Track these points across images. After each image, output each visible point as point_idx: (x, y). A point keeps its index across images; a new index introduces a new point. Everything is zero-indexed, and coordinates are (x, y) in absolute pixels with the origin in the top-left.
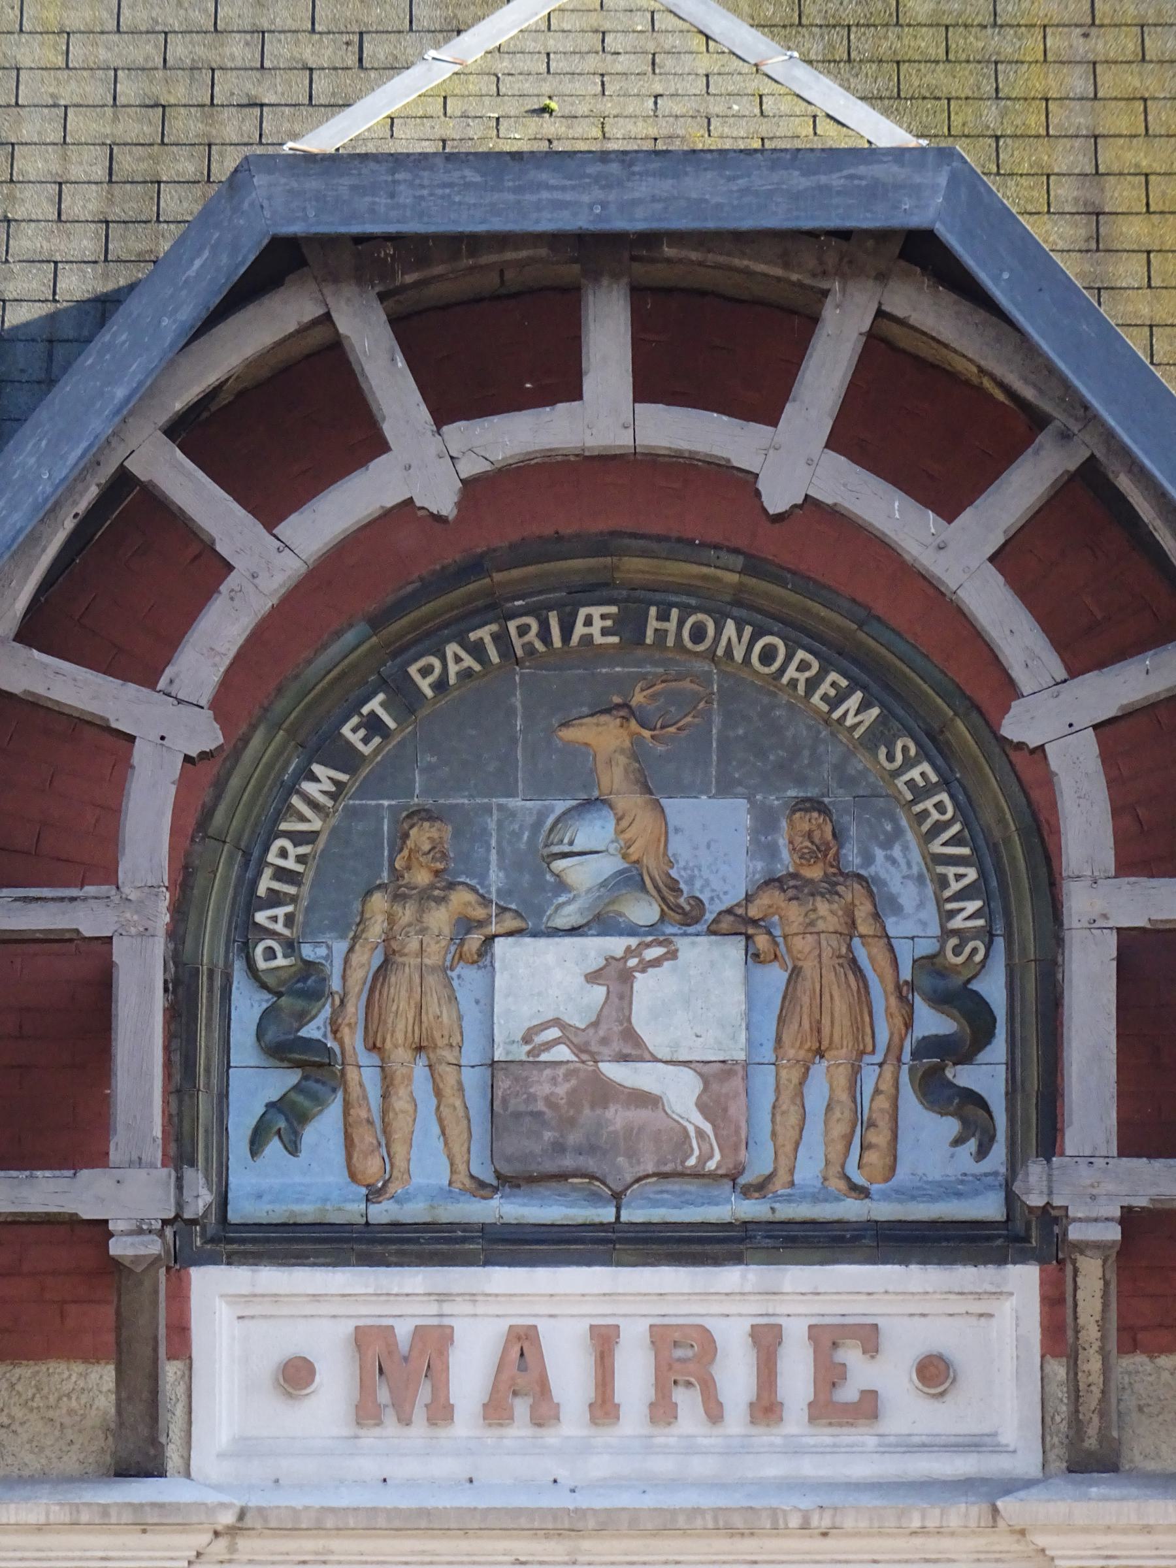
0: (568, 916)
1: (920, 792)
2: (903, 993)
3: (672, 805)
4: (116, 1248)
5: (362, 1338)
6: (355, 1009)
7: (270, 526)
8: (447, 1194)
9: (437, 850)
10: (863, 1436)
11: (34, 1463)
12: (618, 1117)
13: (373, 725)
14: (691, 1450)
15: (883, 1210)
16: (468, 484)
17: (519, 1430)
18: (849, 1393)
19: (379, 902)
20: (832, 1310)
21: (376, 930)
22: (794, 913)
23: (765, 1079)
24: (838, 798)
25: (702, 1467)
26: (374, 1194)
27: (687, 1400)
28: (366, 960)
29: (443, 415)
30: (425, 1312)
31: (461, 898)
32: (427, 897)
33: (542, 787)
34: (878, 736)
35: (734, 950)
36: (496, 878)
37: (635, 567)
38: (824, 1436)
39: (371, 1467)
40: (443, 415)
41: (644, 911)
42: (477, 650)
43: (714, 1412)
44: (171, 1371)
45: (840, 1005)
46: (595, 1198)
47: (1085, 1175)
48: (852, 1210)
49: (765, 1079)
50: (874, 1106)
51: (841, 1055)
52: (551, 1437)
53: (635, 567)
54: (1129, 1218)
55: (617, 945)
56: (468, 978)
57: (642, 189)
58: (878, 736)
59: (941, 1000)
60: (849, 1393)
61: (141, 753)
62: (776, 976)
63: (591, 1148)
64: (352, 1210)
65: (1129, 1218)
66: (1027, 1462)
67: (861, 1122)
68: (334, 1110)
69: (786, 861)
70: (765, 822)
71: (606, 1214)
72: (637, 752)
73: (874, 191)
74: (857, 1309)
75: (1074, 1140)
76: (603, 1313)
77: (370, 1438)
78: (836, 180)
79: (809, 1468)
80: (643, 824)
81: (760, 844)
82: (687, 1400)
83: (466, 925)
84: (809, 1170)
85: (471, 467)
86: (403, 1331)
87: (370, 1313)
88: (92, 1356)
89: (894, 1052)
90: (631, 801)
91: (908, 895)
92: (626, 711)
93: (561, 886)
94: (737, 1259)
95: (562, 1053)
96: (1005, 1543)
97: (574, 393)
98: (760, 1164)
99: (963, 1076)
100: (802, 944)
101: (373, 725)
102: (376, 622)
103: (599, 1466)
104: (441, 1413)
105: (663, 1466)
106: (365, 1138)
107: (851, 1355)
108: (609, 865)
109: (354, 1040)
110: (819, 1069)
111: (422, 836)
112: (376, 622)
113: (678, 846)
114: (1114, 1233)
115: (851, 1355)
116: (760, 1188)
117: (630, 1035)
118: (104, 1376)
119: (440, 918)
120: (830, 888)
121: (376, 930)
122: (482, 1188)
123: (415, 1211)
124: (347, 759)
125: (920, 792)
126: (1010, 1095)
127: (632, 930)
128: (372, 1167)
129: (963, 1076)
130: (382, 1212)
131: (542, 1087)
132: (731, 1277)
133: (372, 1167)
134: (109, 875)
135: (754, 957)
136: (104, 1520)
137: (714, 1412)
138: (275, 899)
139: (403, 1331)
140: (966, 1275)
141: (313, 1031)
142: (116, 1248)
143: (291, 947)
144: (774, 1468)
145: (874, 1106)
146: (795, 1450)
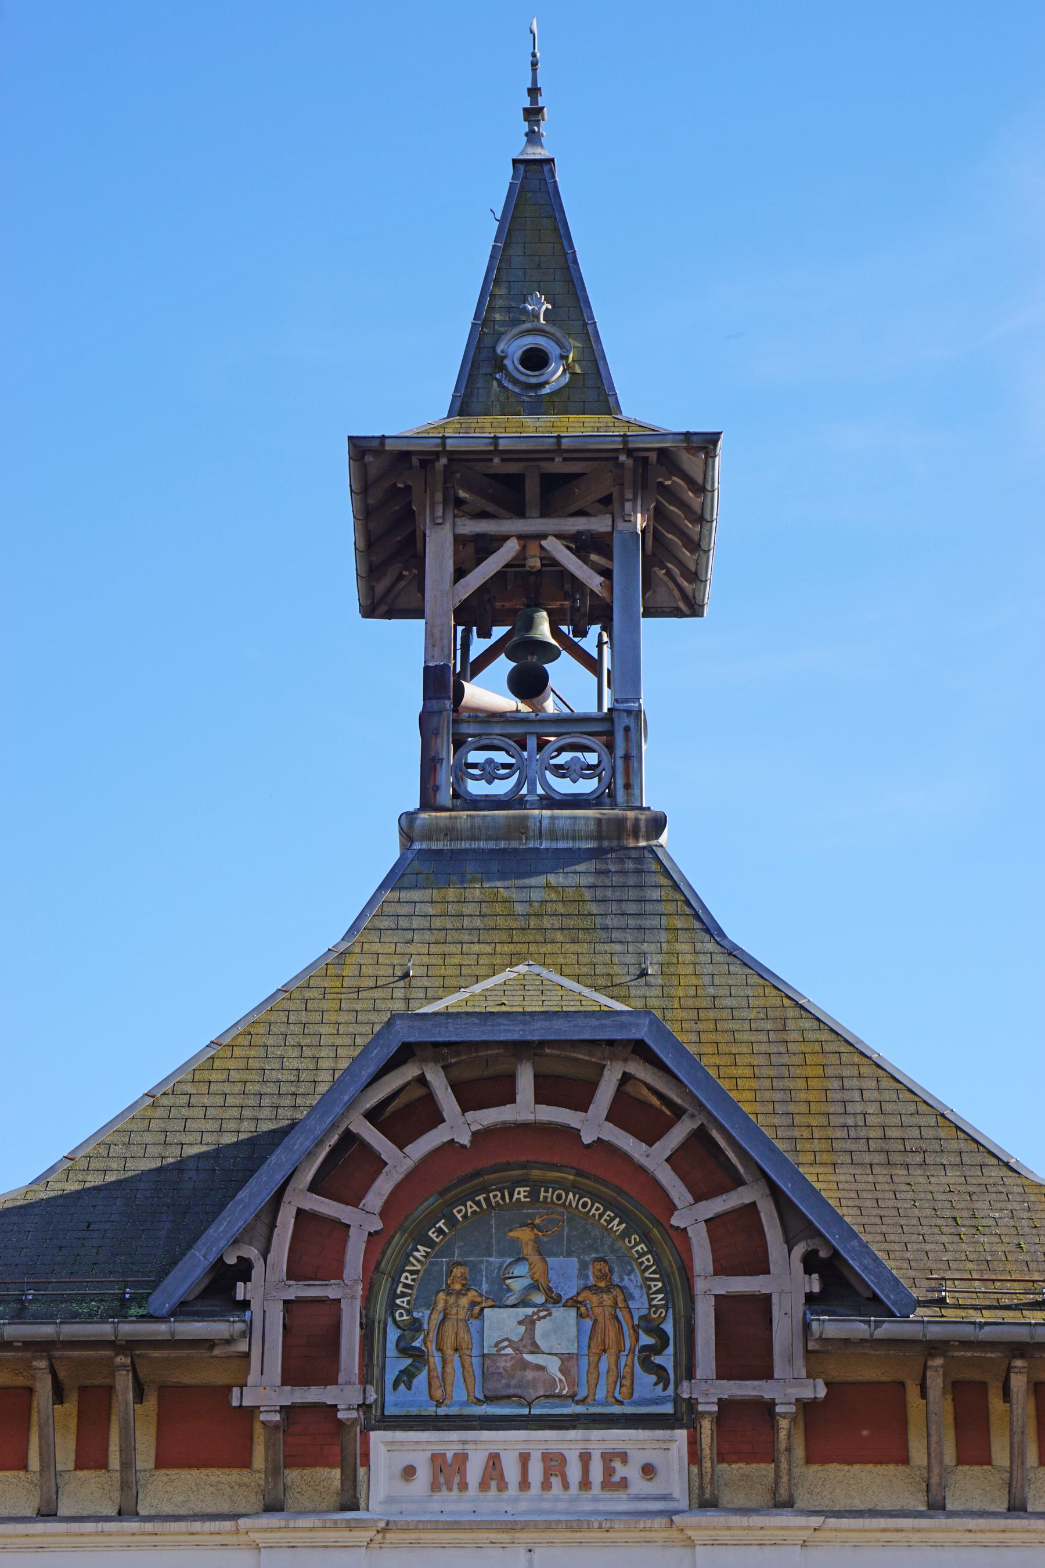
0: (512, 1300)
1: (641, 1255)
2: (635, 1329)
3: (550, 1260)
4: (341, 1415)
5: (434, 1457)
6: (433, 1335)
7: (401, 1148)
8: (466, 1404)
9: (463, 1277)
10: (621, 1495)
11: (309, 1506)
12: (530, 1375)
13: (440, 1231)
14: (556, 1500)
15: (628, 1410)
16: (475, 1134)
17: (493, 1492)
18: (616, 1478)
19: (442, 1295)
20: (610, 1446)
21: (440, 1306)
22: (595, 1299)
23: (584, 1362)
24: (610, 1257)
25: (561, 1506)
26: (439, 1404)
27: (556, 1481)
28: (437, 1317)
29: (464, 1109)
30: (458, 1448)
31: (472, 1294)
32: (459, 1294)
33: (501, 1254)
34: (626, 1234)
35: (573, 1313)
36: (485, 1287)
37: (536, 1173)
38: (607, 1495)
39: (436, 1507)
40: (464, 1109)
41: (539, 1298)
42: (478, 1204)
43: (566, 1486)
44: (362, 1471)
45: (612, 1334)
46: (522, 1406)
47: (704, 1386)
48: (617, 1409)
49: (584, 1362)
50: (625, 1371)
51: (613, 1351)
52: (505, 1495)
53: (536, 1173)
54: (721, 1402)
55: (529, 1311)
56: (474, 1324)
57: (538, 1025)
58: (626, 1234)
59: (649, 1332)
60: (616, 1478)
61: (352, 1231)
62: (588, 1323)
63: (520, 1386)
64: (431, 1410)
65: (721, 1402)
66: (684, 1504)
67: (620, 1377)
68: (424, 1373)
69: (592, 1281)
70: (584, 1266)
71: (526, 1411)
72: (537, 1241)
73: (623, 1026)
74: (619, 1446)
75: (699, 1373)
76: (524, 1448)
77: (437, 1496)
78: (607, 1022)
79: (601, 1507)
80: (539, 1267)
81: (582, 1274)
82: (556, 1481)
83: (473, 1304)
84: (601, 1394)
85: (475, 1127)
86: (450, 1455)
87: (437, 1448)
88: (332, 1466)
89: (632, 1350)
90: (535, 1258)
91: (636, 1292)
92: (533, 1226)
93: (509, 1289)
94: (574, 1428)
95: (509, 1351)
96: (675, 1534)
97: (512, 1100)
98: (582, 1393)
99: (657, 1360)
100: (598, 1311)
101: (440, 1231)
102: (441, 1194)
103: (523, 1506)
104: (464, 1486)
105: (546, 1506)
106: (436, 1383)
107: (617, 1464)
108: (527, 1282)
109: (432, 1347)
110: (604, 1358)
111: (458, 1271)
112: (441, 1194)
113: (552, 1274)
114: (715, 1408)
115: (617, 1464)
116: (583, 1401)
117: (534, 1344)
118: (337, 1473)
119: (464, 1301)
120: (608, 1290)
121: (440, 1306)
122: (479, 1402)
123: (454, 1411)
124: (431, 1244)
125: (641, 1255)
126: (675, 1367)
127: (535, 1306)
128: (438, 1394)
129: (657, 1360)
130: (442, 1411)
131: (502, 1363)
132: (572, 1434)
133: (438, 1394)
134: (340, 1276)
135: (580, 1316)
136: (335, 1526)
137: (566, 1486)
138: (403, 1295)
139: (450, 1455)
140: (659, 1433)
141: (416, 1344)
142: (341, 1415)
143: (409, 1312)
144: (588, 1507)
145: (625, 1371)
146: (596, 1500)
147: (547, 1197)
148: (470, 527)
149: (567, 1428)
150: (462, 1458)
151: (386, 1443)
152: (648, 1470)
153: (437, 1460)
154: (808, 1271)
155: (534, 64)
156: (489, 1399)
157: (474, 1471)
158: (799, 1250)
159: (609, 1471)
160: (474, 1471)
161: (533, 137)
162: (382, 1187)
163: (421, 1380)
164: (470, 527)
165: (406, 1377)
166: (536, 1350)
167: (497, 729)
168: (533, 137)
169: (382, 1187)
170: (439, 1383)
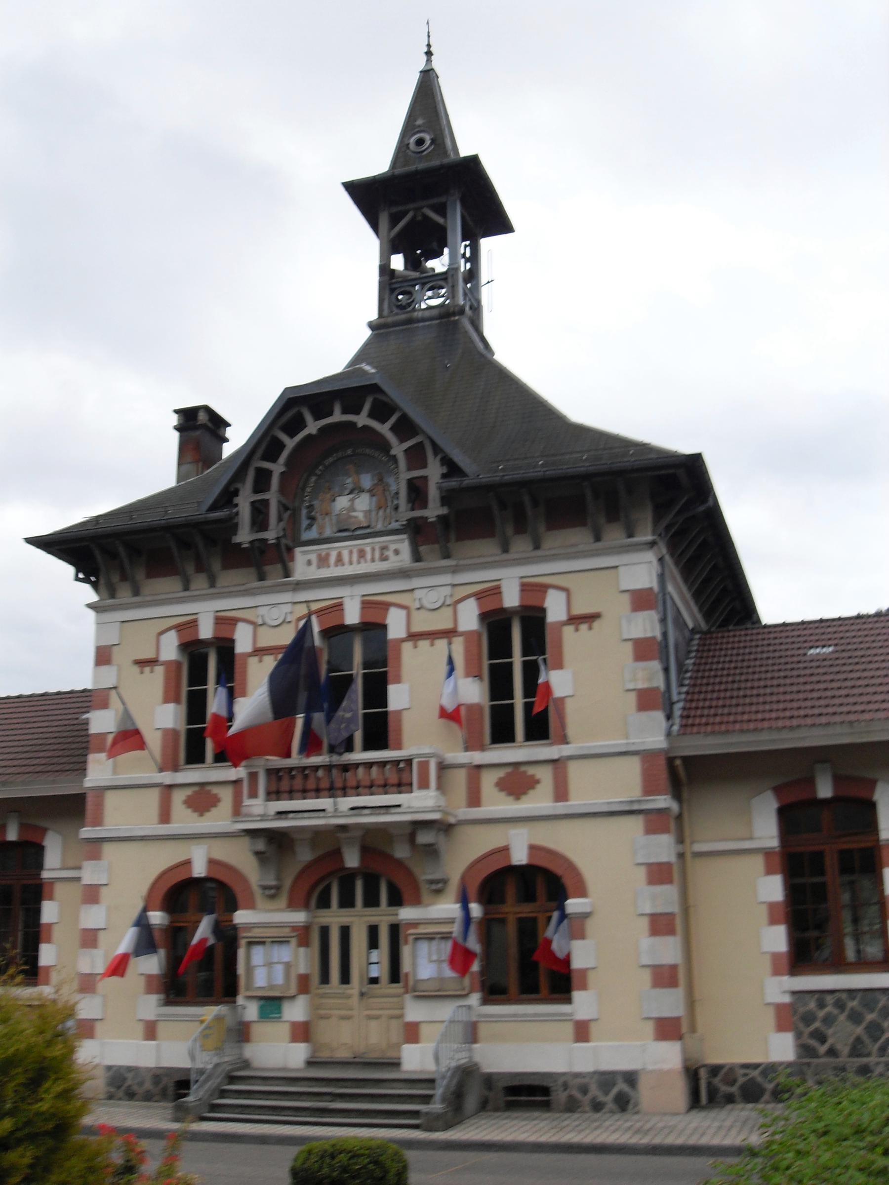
12: (353, 520)
147: (266, 503)
148: (394, 210)
149: (366, 538)
150: (328, 555)
151: (302, 552)
152: (397, 552)
153: (319, 556)
154: (442, 465)
155: (429, 36)
156: (340, 531)
157: (333, 559)
158: (439, 457)
159: (382, 554)
160: (333, 559)
161: (429, 61)
162: (375, 424)
163: (315, 528)
164: (394, 210)
165: (310, 527)
166: (355, 511)
167: (406, 284)
168: (429, 61)
169: (375, 424)
170: (321, 528)
